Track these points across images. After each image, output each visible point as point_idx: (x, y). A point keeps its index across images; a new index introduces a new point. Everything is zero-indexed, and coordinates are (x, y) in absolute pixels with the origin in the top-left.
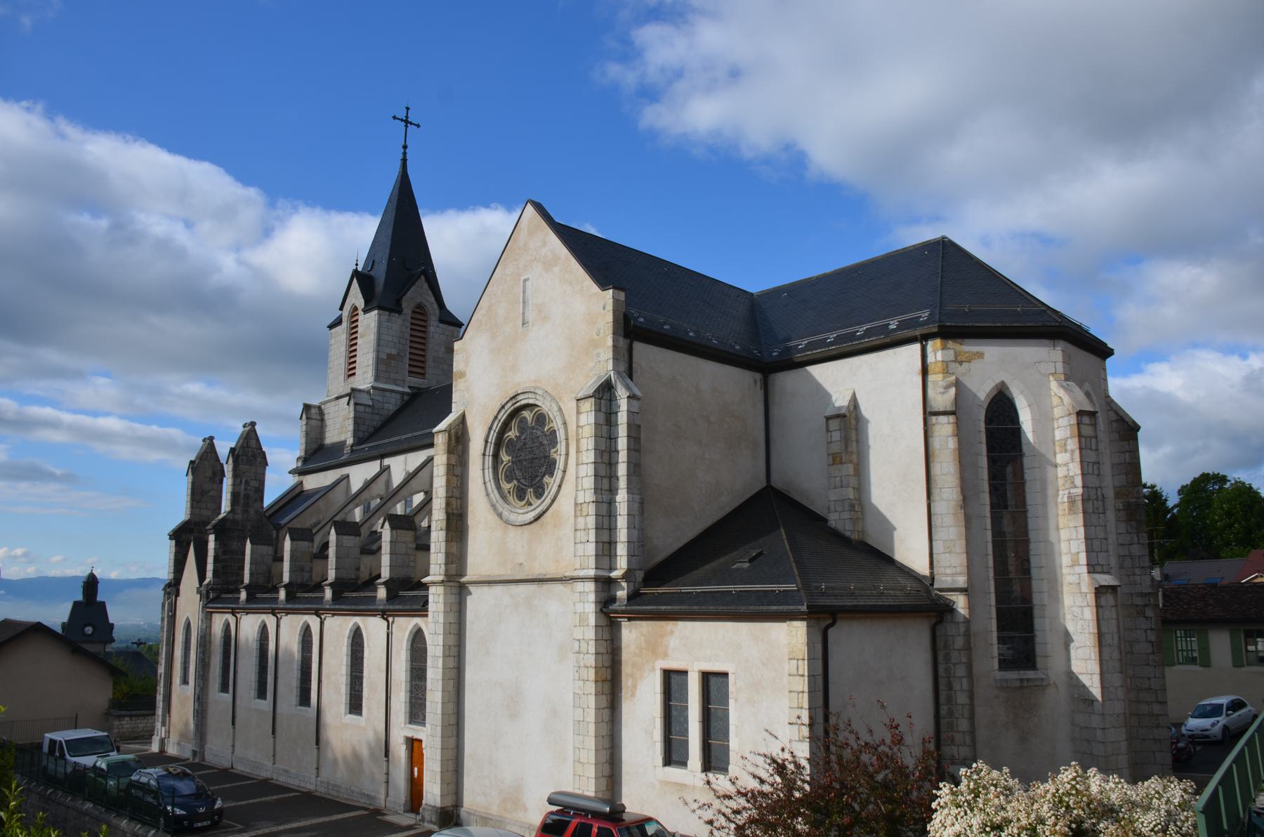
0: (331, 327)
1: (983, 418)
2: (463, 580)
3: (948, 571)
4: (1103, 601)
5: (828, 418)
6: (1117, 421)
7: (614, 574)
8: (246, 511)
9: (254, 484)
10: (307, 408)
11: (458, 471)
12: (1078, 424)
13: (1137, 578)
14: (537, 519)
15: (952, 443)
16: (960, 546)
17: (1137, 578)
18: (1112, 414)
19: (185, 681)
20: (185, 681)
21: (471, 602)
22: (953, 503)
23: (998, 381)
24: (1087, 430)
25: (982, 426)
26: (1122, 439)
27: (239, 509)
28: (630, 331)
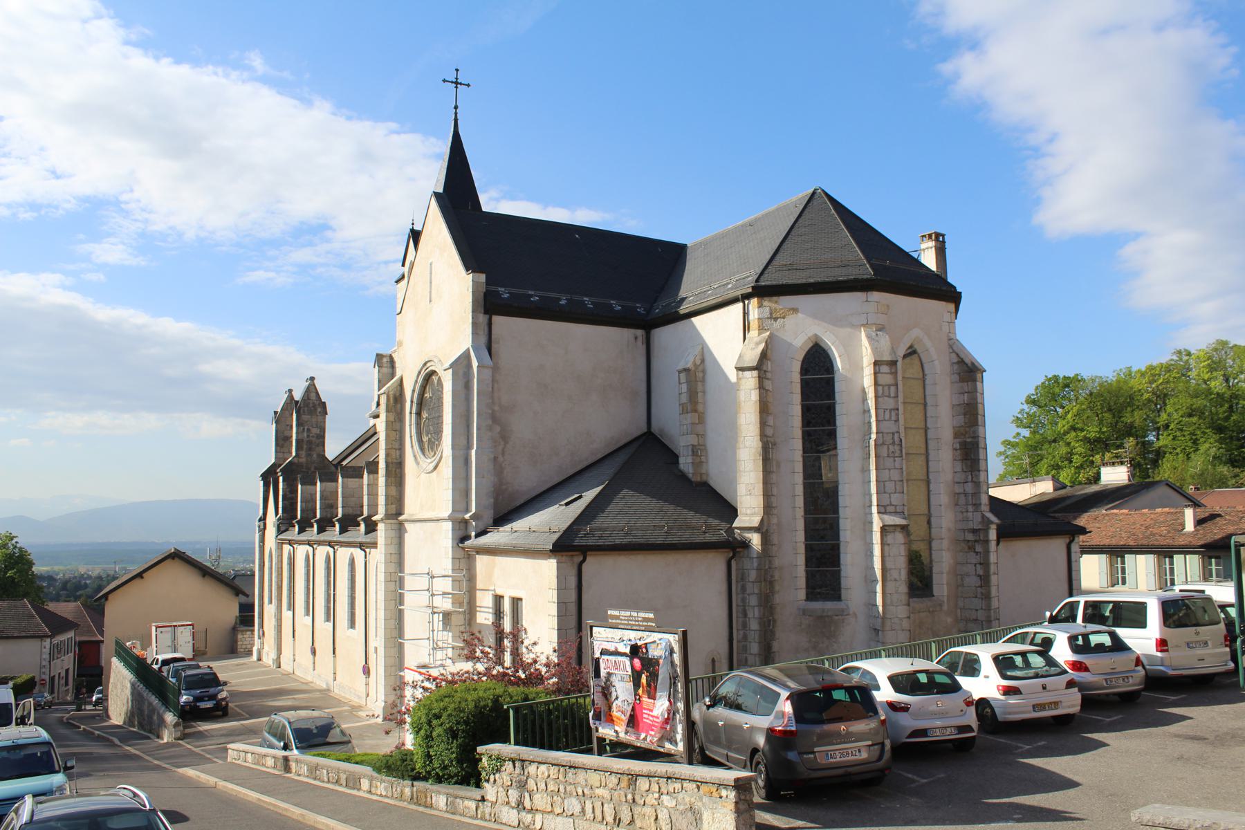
0: (397, 282)
1: (798, 369)
2: (401, 518)
3: (749, 512)
4: (889, 539)
5: (680, 372)
6: (958, 363)
7: (467, 516)
8: (309, 455)
9: (315, 431)
10: (379, 357)
11: (397, 426)
12: (875, 373)
13: (970, 514)
14: (435, 468)
15: (755, 396)
16: (759, 489)
17: (970, 514)
18: (954, 355)
19: (270, 602)
20: (270, 602)
21: (409, 539)
22: (753, 451)
23: (810, 334)
24: (886, 379)
25: (796, 377)
26: (962, 380)
27: (303, 453)
28: (489, 305)
